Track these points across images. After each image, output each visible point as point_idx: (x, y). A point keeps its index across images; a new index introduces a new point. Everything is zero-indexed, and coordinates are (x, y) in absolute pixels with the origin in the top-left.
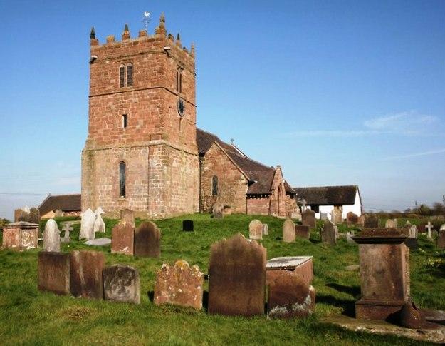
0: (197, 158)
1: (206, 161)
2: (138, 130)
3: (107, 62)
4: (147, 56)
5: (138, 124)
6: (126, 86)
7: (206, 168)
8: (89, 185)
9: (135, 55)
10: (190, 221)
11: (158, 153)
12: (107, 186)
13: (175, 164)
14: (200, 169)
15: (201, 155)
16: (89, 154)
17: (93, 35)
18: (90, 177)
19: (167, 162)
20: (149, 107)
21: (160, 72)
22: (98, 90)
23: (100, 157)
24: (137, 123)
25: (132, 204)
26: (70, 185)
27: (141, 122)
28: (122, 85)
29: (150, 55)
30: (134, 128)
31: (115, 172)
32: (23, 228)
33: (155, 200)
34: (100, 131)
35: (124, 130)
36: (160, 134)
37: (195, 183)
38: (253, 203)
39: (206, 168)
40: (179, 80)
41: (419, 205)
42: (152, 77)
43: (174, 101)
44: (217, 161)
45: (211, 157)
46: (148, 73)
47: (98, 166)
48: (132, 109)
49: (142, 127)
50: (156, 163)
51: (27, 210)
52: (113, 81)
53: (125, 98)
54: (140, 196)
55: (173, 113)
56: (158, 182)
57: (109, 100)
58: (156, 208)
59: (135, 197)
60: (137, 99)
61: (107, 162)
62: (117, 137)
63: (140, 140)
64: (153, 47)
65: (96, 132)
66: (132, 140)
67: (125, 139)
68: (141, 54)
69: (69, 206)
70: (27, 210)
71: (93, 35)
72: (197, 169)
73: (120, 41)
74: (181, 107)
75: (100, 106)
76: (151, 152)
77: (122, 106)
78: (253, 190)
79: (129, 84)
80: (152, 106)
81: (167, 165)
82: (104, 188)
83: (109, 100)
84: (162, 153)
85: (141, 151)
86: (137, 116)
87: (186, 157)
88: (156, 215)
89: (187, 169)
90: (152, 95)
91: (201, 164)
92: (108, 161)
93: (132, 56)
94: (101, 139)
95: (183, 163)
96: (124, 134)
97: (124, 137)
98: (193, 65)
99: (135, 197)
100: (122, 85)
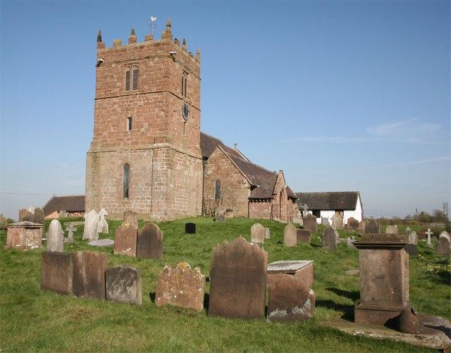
11: (162, 156)
12: (111, 187)
13: (178, 167)
15: (205, 159)
16: (94, 156)
17: (100, 39)
19: (171, 165)
22: (104, 94)
23: (105, 158)
26: (74, 185)
31: (119, 174)
32: (27, 227)
34: (105, 133)
38: (255, 207)
40: (184, 84)
43: (179, 105)
47: (103, 168)
50: (160, 166)
51: (31, 210)
55: (177, 117)
61: (111, 164)
69: (73, 206)
70: (31, 210)
71: (100, 39)
72: (200, 173)
73: (126, 45)
74: (186, 111)
78: (255, 194)
79: (135, 87)
89: (191, 173)
98: (198, 70)
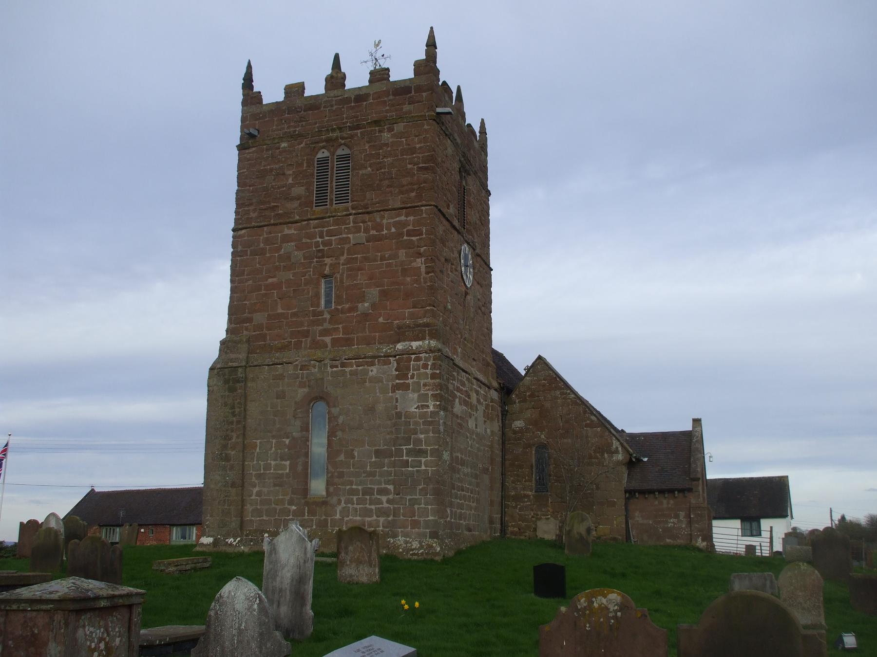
0: (494, 395)
1: (517, 406)
2: (365, 316)
3: (284, 145)
4: (390, 130)
5: (364, 301)
6: (349, 188)
7: (518, 424)
8: (227, 459)
9: (358, 127)
10: (553, 566)
14: (503, 426)
18: (227, 438)
20: (395, 256)
21: (426, 169)
24: (362, 298)
25: (345, 512)
27: (374, 293)
28: (322, 199)
29: (399, 127)
30: (353, 309)
33: (413, 502)
35: (327, 316)
36: (427, 325)
37: (492, 461)
39: (518, 424)
41: (837, 517)
42: (405, 181)
44: (548, 405)
45: (532, 396)
46: (394, 171)
48: (348, 261)
49: (373, 306)
52: (299, 190)
53: (330, 233)
54: (367, 492)
56: (421, 453)
57: (286, 239)
58: (415, 524)
59: (353, 492)
60: (362, 235)
62: (306, 334)
63: (368, 342)
64: (406, 108)
65: (250, 320)
66: (348, 342)
67: (328, 339)
68: (376, 123)
72: (496, 426)
75: (262, 252)
76: (403, 373)
77: (322, 255)
80: (402, 253)
81: (445, 409)
82: (267, 467)
83: (286, 239)
84: (433, 376)
85: (374, 371)
86: (361, 279)
87: (477, 393)
88: (415, 545)
90: (405, 224)
91: (504, 413)
92: (281, 396)
93: (351, 129)
94: (263, 337)
95: (472, 407)
96: (326, 325)
97: (325, 333)
99: (353, 492)
100: (322, 199)
